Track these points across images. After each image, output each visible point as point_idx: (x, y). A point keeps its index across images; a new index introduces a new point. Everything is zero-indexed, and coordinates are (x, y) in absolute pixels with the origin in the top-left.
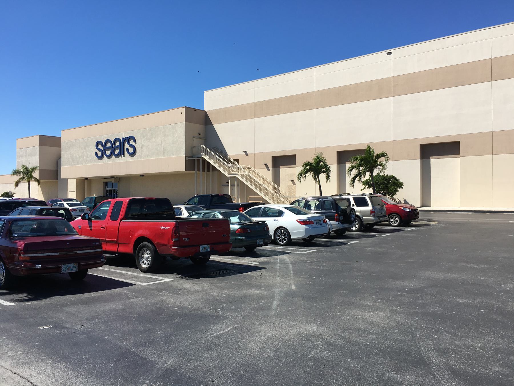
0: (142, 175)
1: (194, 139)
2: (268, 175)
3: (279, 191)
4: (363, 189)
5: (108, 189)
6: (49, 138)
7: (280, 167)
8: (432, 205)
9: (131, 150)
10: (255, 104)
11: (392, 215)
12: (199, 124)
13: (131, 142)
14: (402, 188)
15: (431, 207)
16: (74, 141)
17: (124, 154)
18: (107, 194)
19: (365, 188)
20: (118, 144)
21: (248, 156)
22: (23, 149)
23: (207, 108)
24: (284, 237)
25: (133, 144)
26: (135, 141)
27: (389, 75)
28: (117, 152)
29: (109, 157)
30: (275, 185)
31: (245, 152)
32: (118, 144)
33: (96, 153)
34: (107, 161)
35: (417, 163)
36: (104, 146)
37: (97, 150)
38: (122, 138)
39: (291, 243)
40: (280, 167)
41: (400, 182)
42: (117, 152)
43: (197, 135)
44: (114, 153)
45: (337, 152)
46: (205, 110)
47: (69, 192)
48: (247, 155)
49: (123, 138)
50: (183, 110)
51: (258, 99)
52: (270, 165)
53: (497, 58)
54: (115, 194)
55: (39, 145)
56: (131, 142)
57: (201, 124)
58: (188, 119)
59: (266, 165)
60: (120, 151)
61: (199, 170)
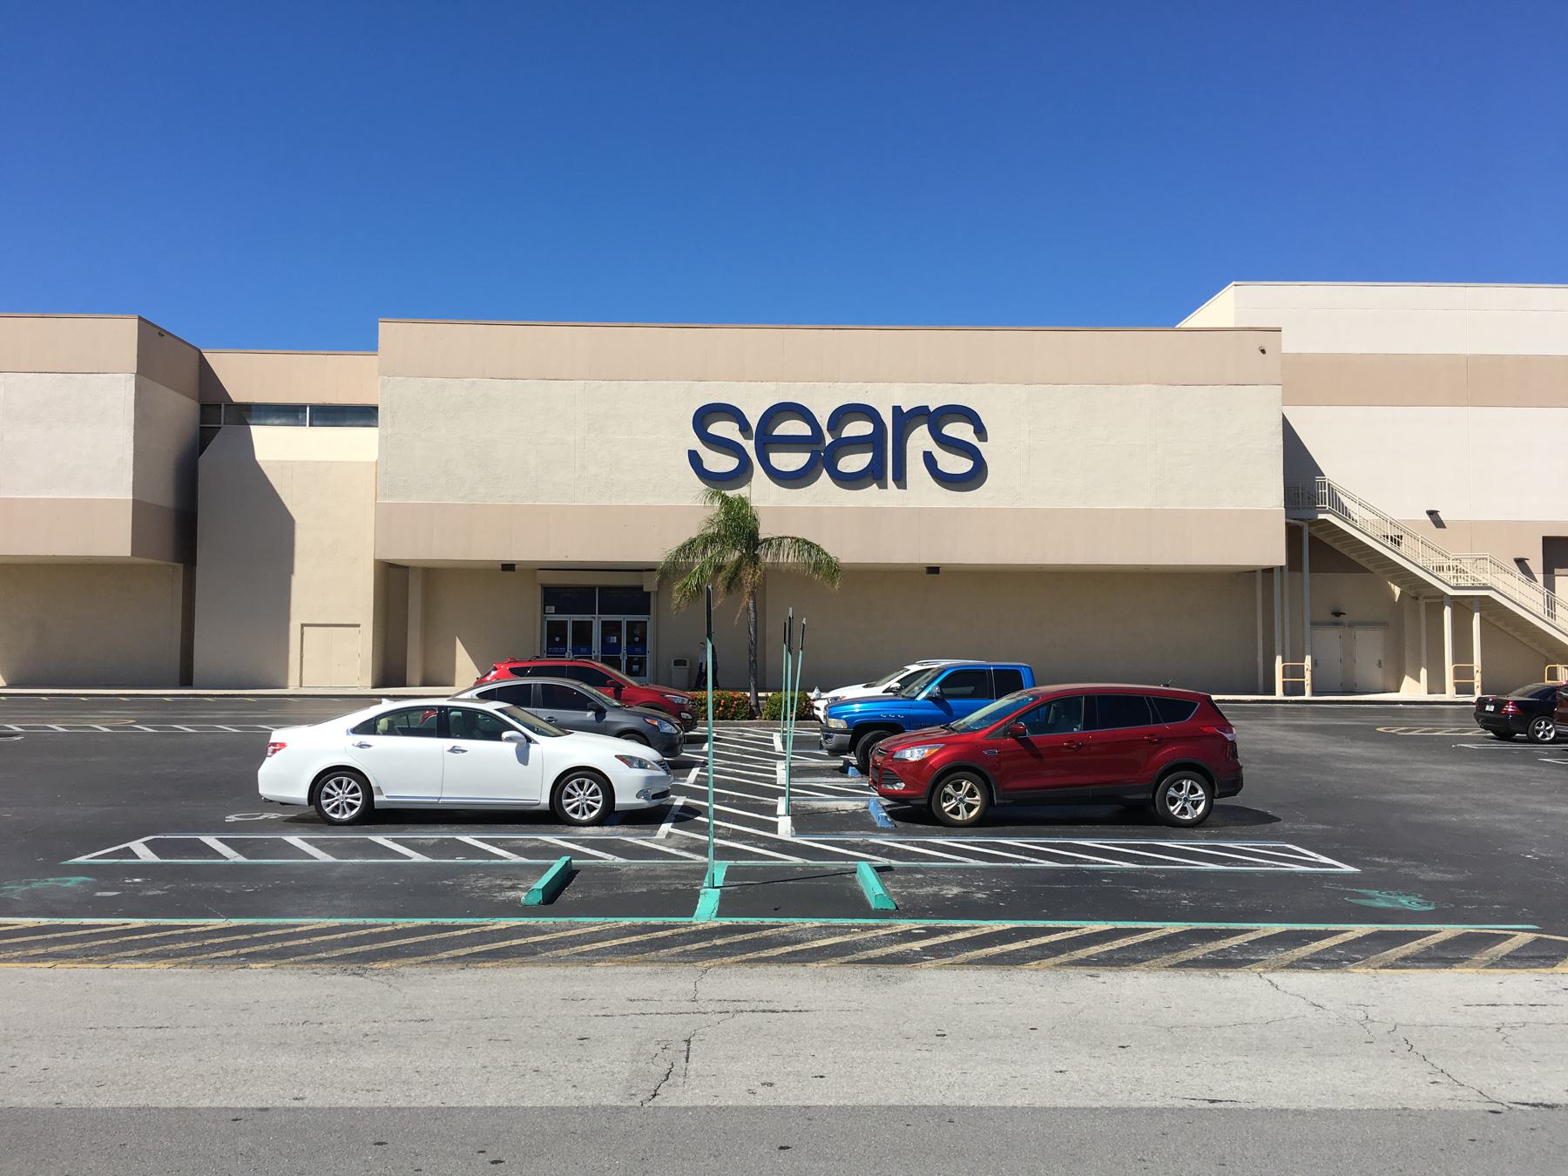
0: (933, 570)
7: (1557, 571)
8: (456, 683)
9: (957, 465)
11: (1531, 725)
12: (185, 395)
15: (453, 686)
21: (1445, 527)
24: (592, 801)
31: (1432, 513)
37: (696, 443)
39: (611, 815)
40: (1557, 571)
47: (303, 626)
48: (1439, 523)
54: (614, 640)
57: (193, 399)
58: (147, 369)
59: (1520, 562)
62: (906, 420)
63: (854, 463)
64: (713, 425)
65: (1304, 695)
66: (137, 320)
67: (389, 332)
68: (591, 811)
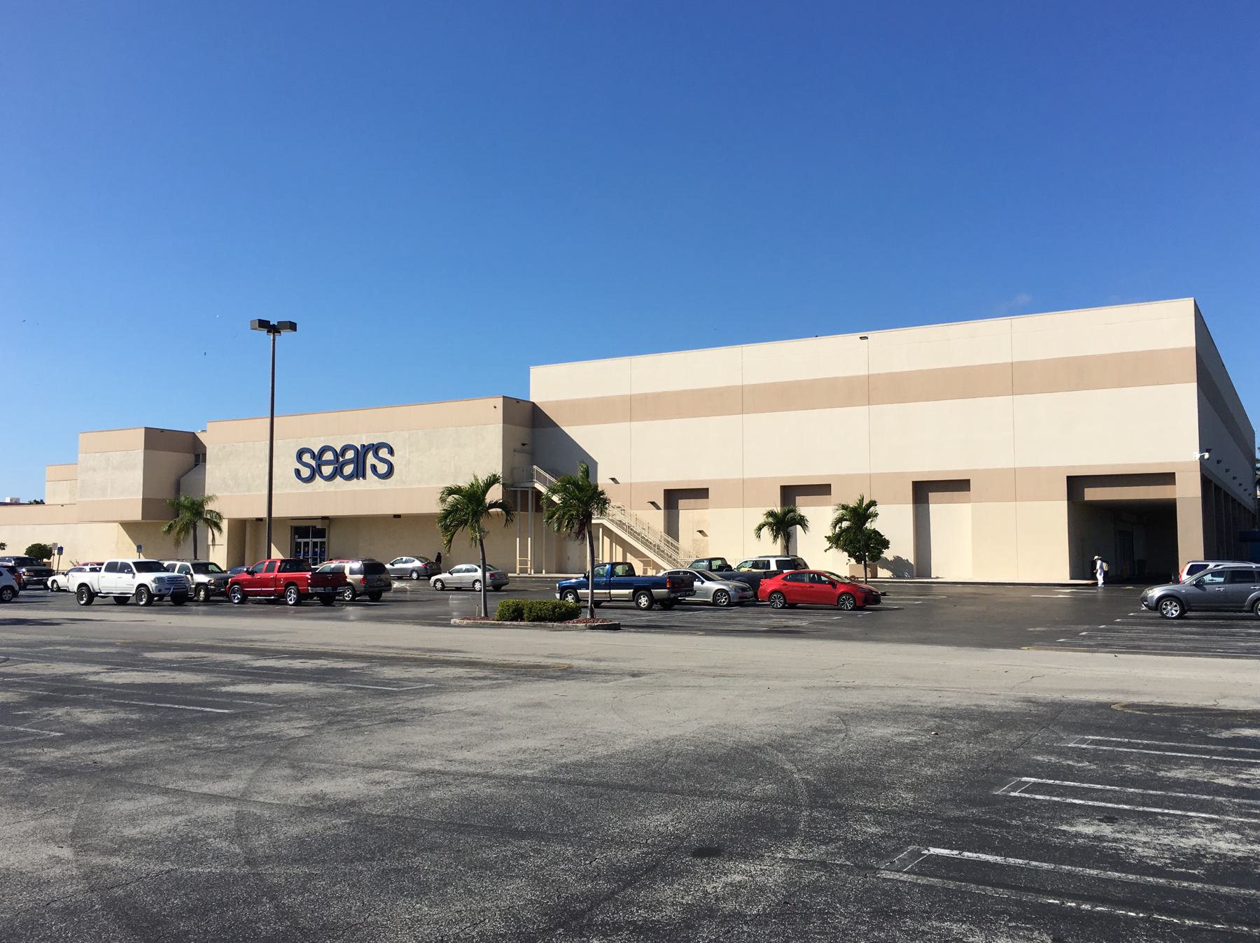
0: (397, 516)
1: (516, 453)
2: (657, 519)
3: (677, 548)
4: (828, 549)
5: (299, 540)
6: (163, 433)
9: (382, 468)
10: (631, 398)
13: (383, 453)
14: (888, 548)
16: (241, 445)
17: (364, 476)
18: (296, 550)
19: (830, 548)
20: (350, 455)
22: (98, 454)
23: (535, 398)
25: (388, 457)
26: (391, 452)
27: (864, 372)
28: (348, 469)
29: (330, 478)
30: (670, 539)
32: (350, 455)
33: (298, 472)
34: (322, 487)
35: (908, 509)
36: (318, 457)
38: (361, 445)
41: (885, 539)
42: (348, 469)
43: (519, 446)
44: (342, 473)
45: (781, 486)
46: (531, 401)
49: (363, 446)
50: (499, 402)
51: (637, 390)
52: (661, 503)
53: (1021, 364)
55: (145, 449)
56: (383, 453)
59: (653, 503)
60: (356, 468)
61: (525, 509)
62: (367, 448)
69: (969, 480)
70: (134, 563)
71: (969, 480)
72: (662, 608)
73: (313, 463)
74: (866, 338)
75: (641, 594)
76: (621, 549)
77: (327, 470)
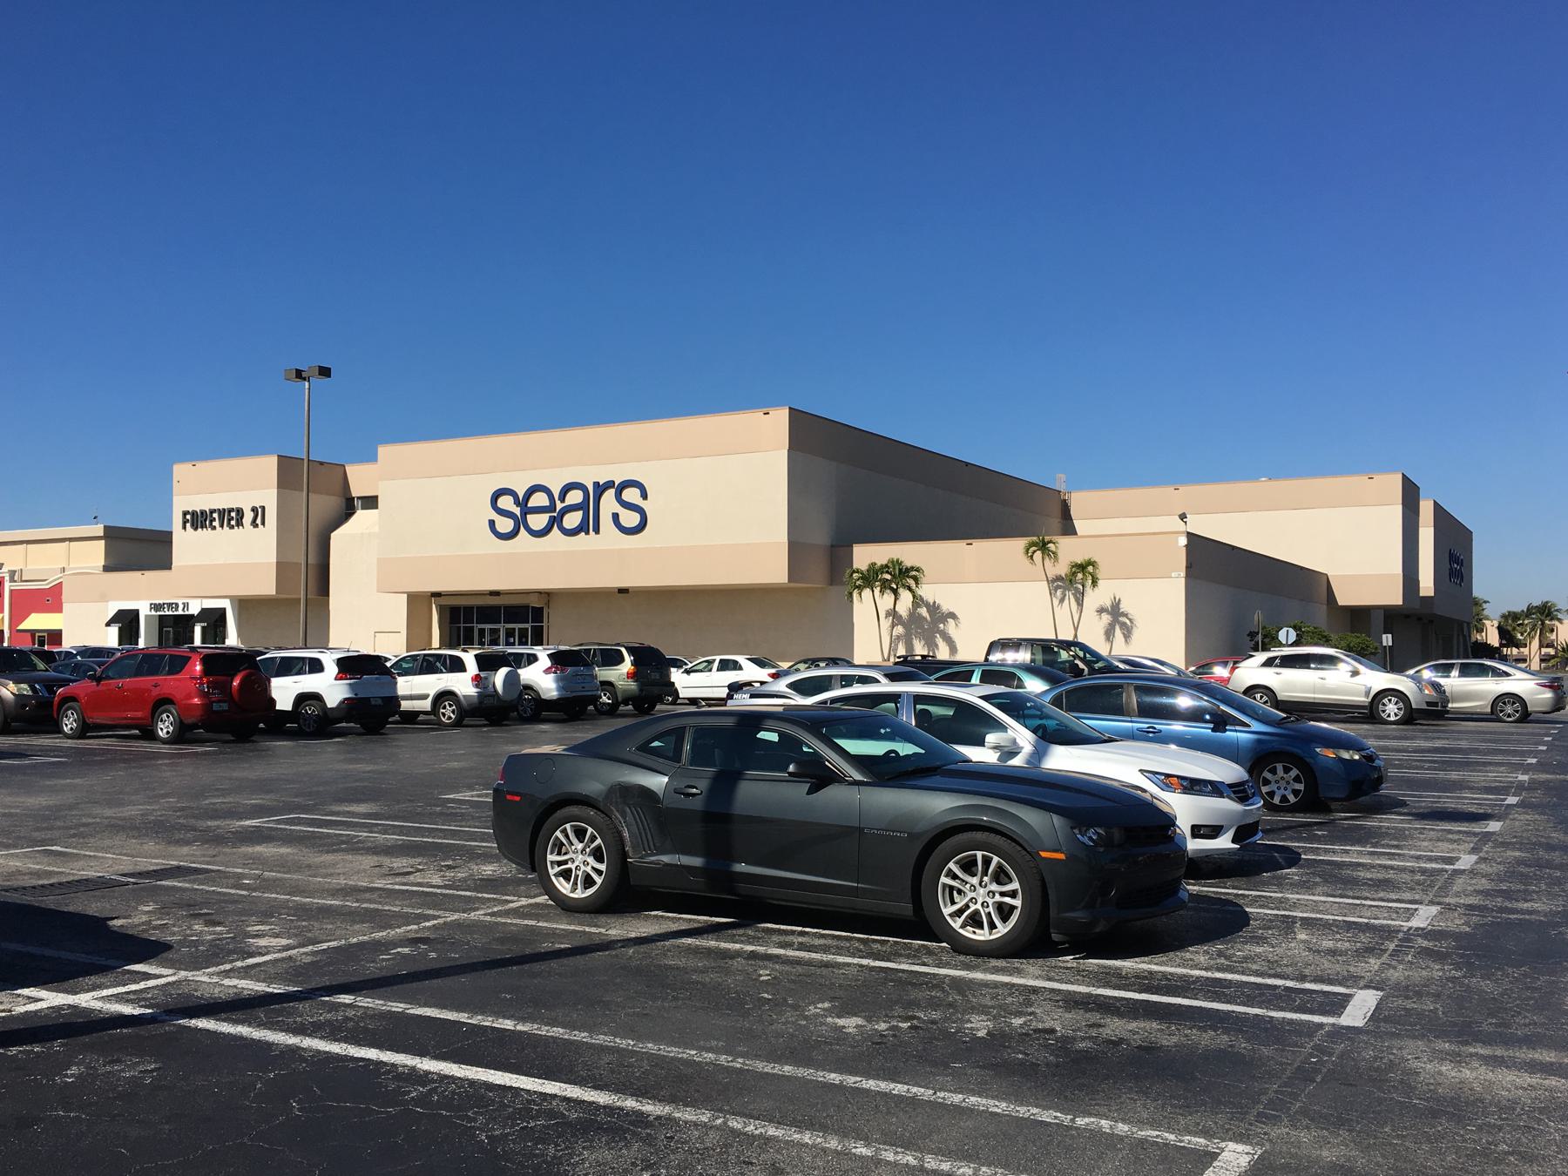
0: (623, 591)
9: (630, 519)
49: (596, 484)
62: (600, 489)
63: (572, 520)
64: (633, 526)
65: (225, 609)
66: (276, 458)
67: (383, 451)
68: (1005, 919)
69: (376, 497)
70: (982, 928)
71: (376, 497)
72: (565, 717)
73: (517, 511)
74: (768, 413)
75: (67, 710)
76: (33, 616)
77: (538, 521)
